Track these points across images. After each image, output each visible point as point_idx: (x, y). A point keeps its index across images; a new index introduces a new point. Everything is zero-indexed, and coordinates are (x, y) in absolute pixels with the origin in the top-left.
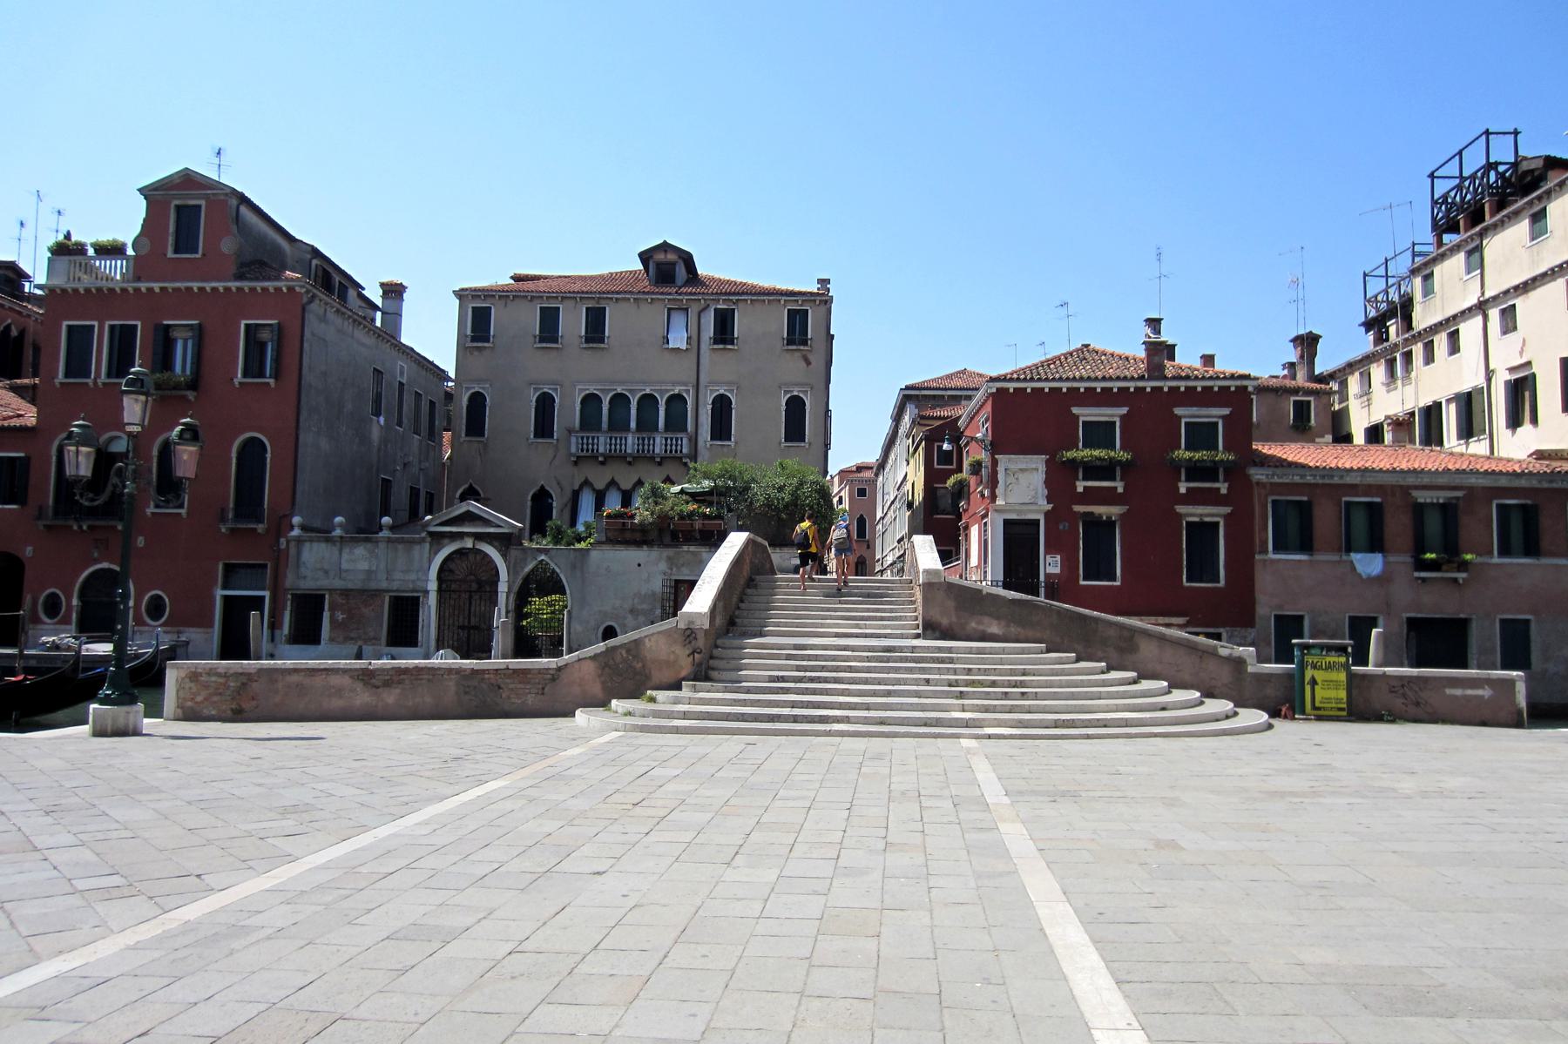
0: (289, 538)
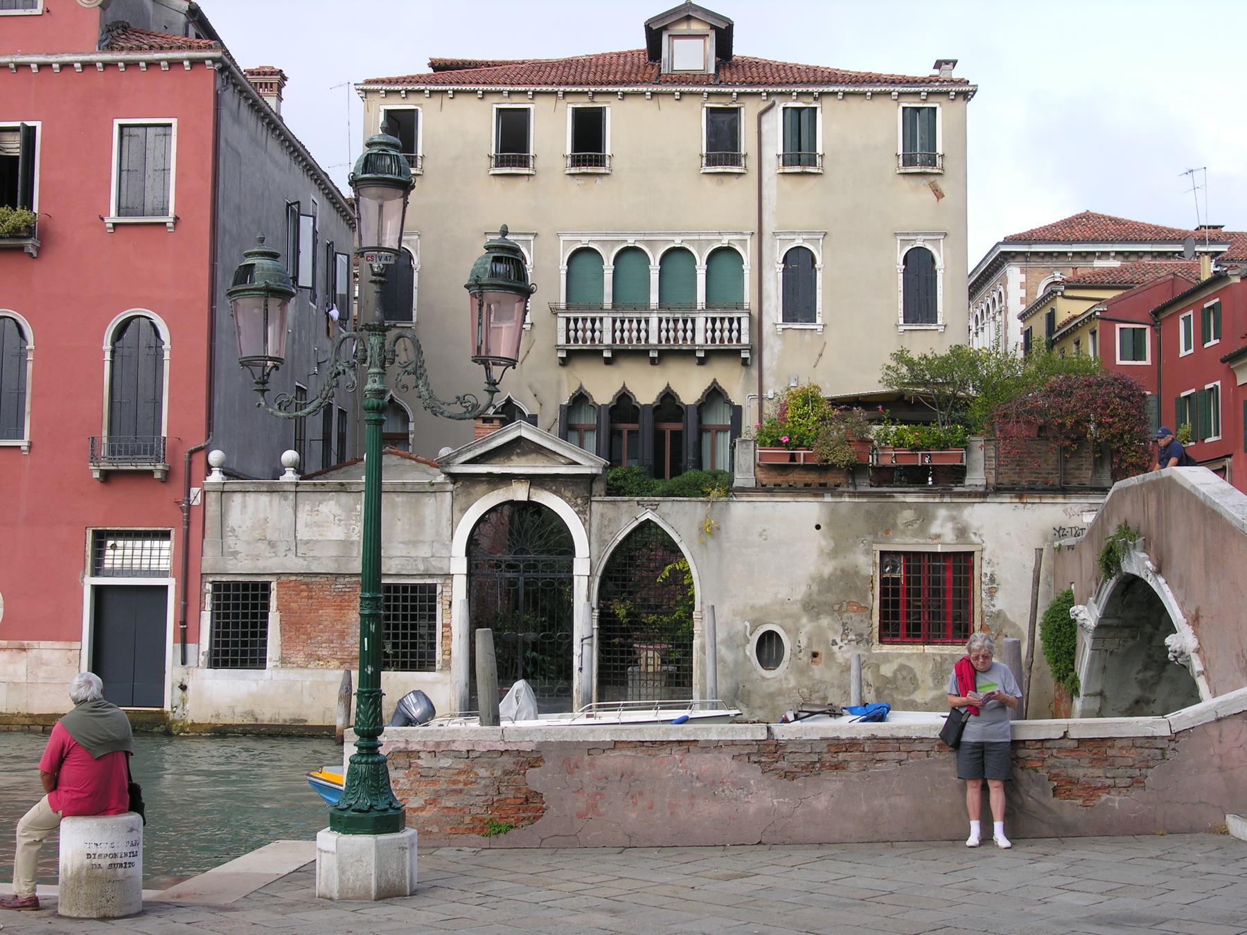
0: (206, 488)
